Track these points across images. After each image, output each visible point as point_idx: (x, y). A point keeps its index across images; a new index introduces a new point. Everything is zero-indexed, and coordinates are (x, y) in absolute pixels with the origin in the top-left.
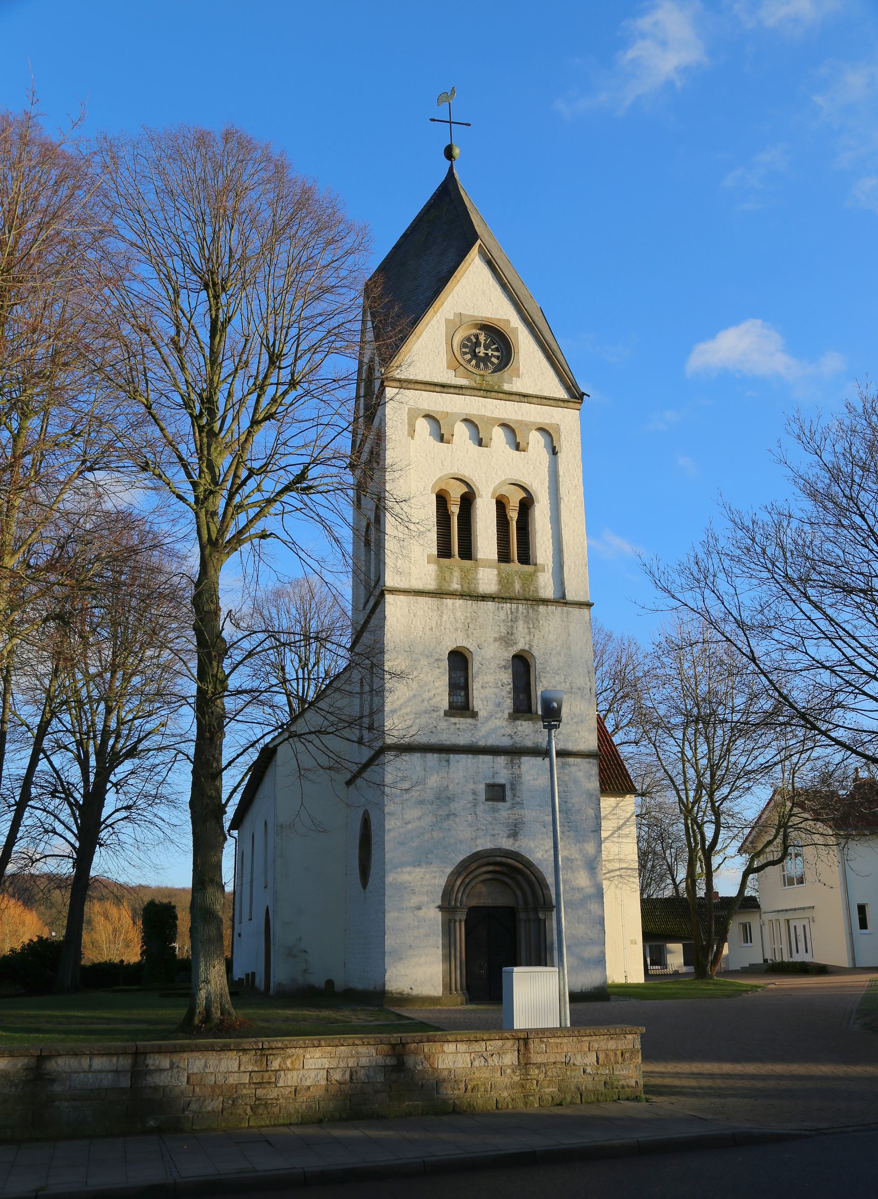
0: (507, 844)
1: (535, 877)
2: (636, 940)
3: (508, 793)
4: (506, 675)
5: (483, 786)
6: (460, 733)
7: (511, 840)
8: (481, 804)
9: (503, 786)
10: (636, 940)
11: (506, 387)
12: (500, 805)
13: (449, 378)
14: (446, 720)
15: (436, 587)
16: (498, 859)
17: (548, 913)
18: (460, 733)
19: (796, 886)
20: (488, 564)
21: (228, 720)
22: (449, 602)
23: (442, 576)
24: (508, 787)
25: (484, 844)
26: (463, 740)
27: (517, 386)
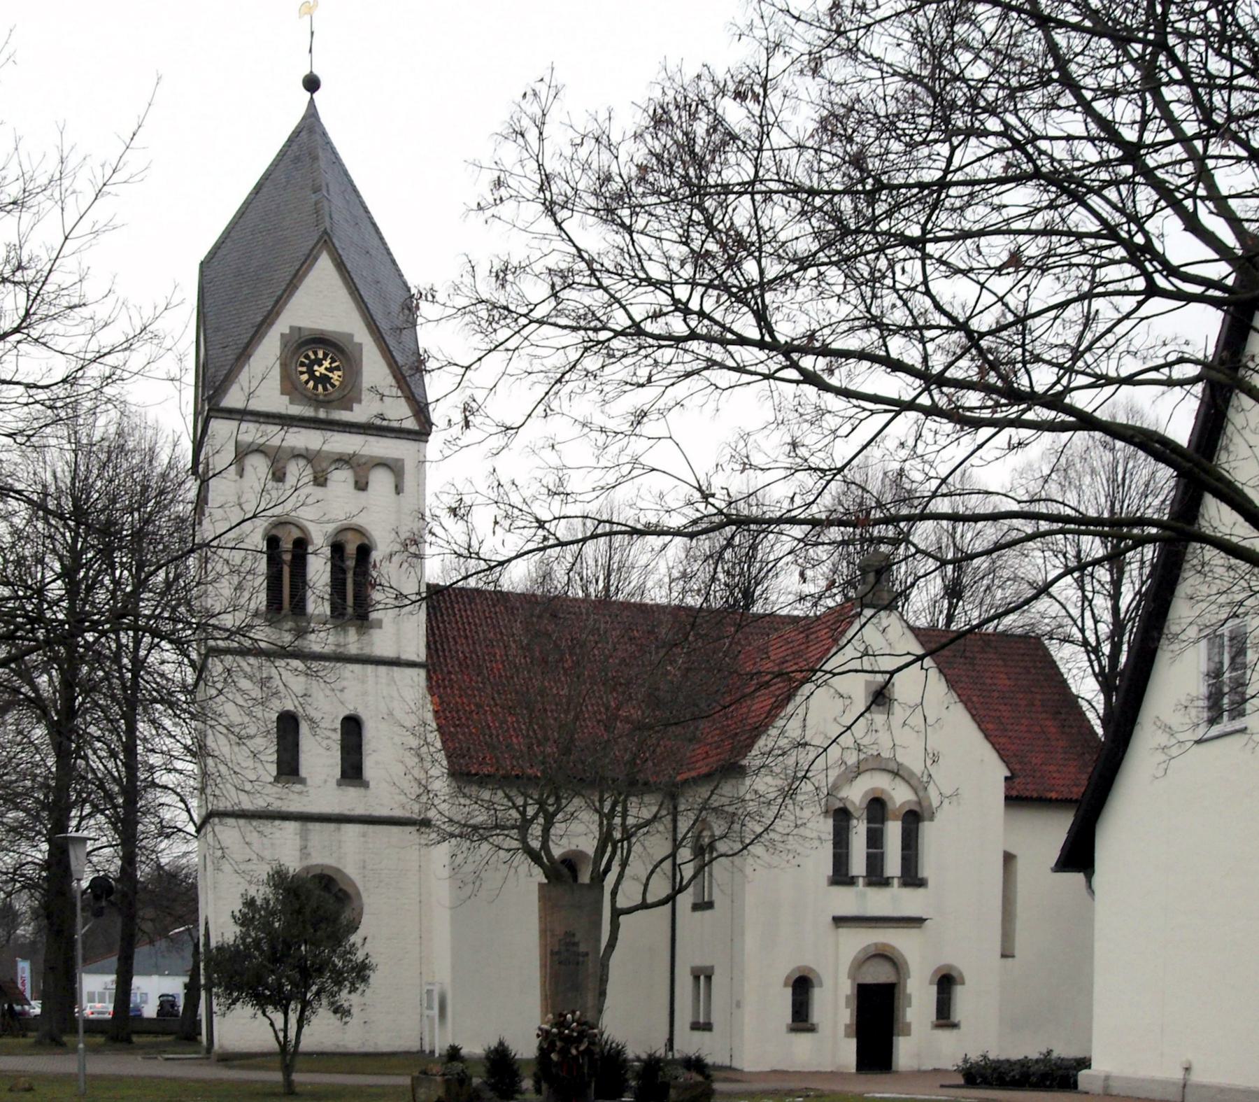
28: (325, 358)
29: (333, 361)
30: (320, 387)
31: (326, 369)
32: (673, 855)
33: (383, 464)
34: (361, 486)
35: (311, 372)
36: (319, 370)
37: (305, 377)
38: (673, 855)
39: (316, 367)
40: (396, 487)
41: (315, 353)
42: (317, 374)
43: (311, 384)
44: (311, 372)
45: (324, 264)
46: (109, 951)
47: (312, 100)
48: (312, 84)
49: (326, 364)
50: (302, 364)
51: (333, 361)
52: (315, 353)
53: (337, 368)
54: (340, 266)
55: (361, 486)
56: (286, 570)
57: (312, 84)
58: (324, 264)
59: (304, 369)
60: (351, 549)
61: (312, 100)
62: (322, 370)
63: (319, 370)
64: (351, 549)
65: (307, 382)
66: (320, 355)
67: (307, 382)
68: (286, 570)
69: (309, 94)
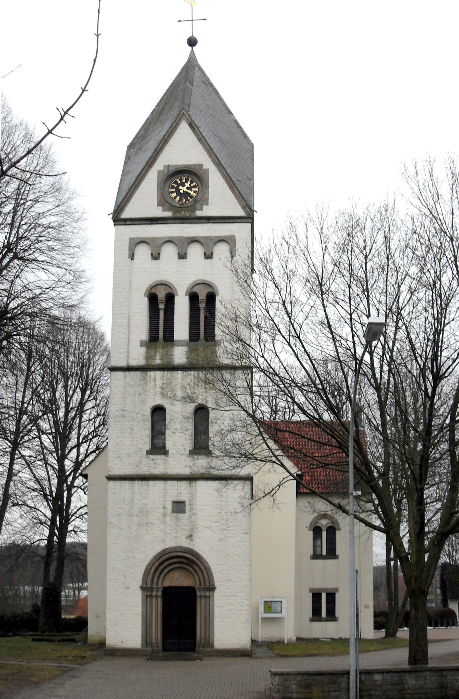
0: (185, 544)
1: (204, 566)
2: (368, 605)
3: (187, 508)
4: (189, 424)
5: (170, 503)
6: (157, 466)
7: (188, 540)
8: (168, 516)
9: (183, 502)
10: (368, 605)
11: (199, 213)
12: (181, 515)
13: (159, 213)
14: (148, 457)
15: (145, 364)
16: (180, 554)
17: (211, 592)
18: (157, 466)
19: (323, 590)
20: (181, 343)
21: (71, 516)
22: (152, 374)
23: (148, 357)
24: (187, 503)
25: (171, 543)
26: (158, 470)
27: (206, 211)
28: (187, 182)
29: (192, 182)
30: (184, 200)
31: (187, 188)
32: (78, 517)
33: (222, 240)
34: (209, 256)
35: (178, 191)
36: (183, 189)
37: (175, 194)
38: (78, 517)
39: (181, 187)
40: (231, 253)
41: (181, 180)
42: (182, 191)
43: (178, 198)
44: (178, 191)
45: (184, 127)
46: (371, 534)
47: (192, 52)
48: (192, 42)
49: (187, 185)
50: (173, 187)
51: (192, 182)
52: (181, 180)
53: (195, 187)
54: (192, 125)
55: (209, 256)
56: (162, 313)
57: (192, 42)
58: (184, 127)
59: (174, 190)
60: (202, 296)
61: (192, 52)
62: (184, 189)
63: (183, 189)
64: (202, 296)
65: (175, 198)
66: (184, 180)
67: (175, 198)
68: (162, 313)
69: (191, 48)
